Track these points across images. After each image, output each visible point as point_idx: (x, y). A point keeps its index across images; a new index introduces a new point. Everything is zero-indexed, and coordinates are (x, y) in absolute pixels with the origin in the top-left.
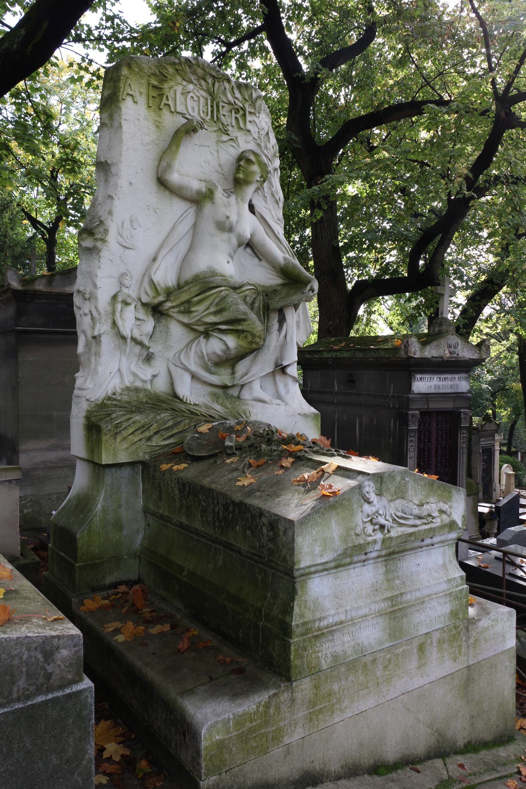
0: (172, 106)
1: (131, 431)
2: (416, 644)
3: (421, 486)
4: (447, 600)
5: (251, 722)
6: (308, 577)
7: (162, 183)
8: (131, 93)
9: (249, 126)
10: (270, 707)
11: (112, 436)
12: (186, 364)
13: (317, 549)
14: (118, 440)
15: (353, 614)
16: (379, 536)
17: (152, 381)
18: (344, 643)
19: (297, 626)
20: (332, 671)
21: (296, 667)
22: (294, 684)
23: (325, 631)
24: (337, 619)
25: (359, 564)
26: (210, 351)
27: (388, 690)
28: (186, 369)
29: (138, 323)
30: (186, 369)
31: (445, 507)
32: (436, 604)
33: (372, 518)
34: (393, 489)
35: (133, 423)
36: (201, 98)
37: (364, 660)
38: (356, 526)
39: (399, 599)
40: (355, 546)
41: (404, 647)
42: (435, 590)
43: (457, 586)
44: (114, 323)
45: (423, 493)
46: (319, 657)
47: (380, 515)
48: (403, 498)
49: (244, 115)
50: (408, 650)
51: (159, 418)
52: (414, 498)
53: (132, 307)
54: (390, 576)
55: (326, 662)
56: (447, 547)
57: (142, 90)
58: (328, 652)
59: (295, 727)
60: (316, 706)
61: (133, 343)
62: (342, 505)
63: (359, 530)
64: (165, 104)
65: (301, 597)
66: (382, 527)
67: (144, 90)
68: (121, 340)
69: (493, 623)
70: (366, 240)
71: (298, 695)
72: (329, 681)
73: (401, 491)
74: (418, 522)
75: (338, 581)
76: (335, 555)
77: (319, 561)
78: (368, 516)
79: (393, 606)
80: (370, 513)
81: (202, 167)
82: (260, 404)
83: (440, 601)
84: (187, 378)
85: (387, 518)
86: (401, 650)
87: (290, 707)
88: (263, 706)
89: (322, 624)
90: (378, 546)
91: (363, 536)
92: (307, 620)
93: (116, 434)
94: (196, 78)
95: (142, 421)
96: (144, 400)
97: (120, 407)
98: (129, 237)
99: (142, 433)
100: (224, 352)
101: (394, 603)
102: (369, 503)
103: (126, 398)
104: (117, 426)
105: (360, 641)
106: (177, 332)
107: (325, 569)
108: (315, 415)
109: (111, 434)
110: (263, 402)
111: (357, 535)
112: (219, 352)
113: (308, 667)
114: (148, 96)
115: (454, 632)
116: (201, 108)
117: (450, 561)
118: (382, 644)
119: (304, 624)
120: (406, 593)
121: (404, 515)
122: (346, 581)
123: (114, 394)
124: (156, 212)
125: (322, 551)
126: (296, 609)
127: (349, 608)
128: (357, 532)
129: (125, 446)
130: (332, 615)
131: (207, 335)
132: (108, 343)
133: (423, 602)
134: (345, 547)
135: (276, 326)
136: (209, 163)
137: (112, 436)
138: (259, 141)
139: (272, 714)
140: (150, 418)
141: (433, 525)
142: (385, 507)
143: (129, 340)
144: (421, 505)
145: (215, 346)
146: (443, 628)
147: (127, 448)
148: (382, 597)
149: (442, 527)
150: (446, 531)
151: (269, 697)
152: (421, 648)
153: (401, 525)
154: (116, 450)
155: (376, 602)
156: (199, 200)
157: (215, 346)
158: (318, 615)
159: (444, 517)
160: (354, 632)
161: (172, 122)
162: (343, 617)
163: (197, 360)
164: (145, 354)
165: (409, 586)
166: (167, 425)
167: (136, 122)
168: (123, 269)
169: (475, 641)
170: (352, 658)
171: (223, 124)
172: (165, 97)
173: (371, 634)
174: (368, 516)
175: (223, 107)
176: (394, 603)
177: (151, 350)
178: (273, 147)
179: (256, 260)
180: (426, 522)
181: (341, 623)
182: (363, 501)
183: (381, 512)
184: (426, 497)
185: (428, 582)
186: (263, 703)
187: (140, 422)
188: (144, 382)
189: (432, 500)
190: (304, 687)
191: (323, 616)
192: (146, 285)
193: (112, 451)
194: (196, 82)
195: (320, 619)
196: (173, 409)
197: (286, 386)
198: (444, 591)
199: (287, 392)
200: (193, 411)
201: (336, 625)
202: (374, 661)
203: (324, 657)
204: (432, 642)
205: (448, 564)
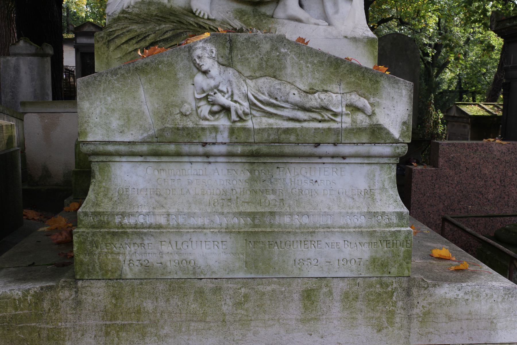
1: (124, 39)
2: (297, 287)
3: (313, 64)
4: (366, 240)
5: (16, 309)
6: (110, 158)
10: (43, 300)
11: (104, 44)
13: (115, 123)
14: (111, 48)
15: (181, 220)
16: (223, 122)
18: (161, 253)
19: (86, 214)
20: (141, 284)
21: (82, 263)
22: (80, 283)
23: (128, 230)
24: (150, 220)
25: (199, 159)
27: (244, 336)
31: (362, 102)
32: (342, 242)
33: (208, 95)
34: (255, 62)
35: (128, 31)
37: (199, 284)
38: (183, 102)
39: (267, 220)
40: (178, 129)
41: (273, 286)
42: (342, 222)
43: (389, 225)
45: (317, 75)
46: (119, 261)
47: (221, 92)
48: (274, 77)
50: (282, 293)
51: (157, 28)
52: (298, 80)
54: (258, 186)
55: (131, 270)
56: (377, 167)
58: (134, 258)
59: (83, 335)
60: (116, 319)
62: (156, 69)
63: (186, 108)
65: (100, 182)
66: (226, 110)
69: (466, 297)
71: (88, 299)
72: (137, 294)
73: (272, 67)
74: (301, 115)
75: (163, 175)
76: (145, 135)
77: (118, 138)
78: (204, 91)
79: (255, 226)
80: (205, 88)
82: (293, 23)
83: (349, 238)
85: (236, 98)
86: (269, 288)
87: (74, 309)
88: (33, 296)
89: (126, 221)
90: (223, 137)
91: (194, 118)
92: (101, 210)
93: (109, 41)
95: (139, 31)
96: (154, 14)
97: (130, 19)
99: (137, 43)
101: (257, 221)
102: (205, 73)
103: (136, 10)
104: (110, 34)
105: (191, 258)
107: (131, 152)
108: (370, 41)
109: (104, 41)
110: (299, 20)
113: (101, 269)
115: (378, 289)
117: (383, 189)
118: (232, 271)
119: (96, 214)
120: (281, 214)
121: (274, 101)
122: (177, 177)
123: (128, 7)
125: (123, 126)
126: (91, 195)
127: (172, 211)
128: (183, 110)
129: (119, 56)
130: (143, 211)
133: (314, 232)
134: (160, 126)
137: (104, 44)
139: (47, 310)
140: (148, 28)
141: (334, 125)
142: (230, 81)
144: (312, 91)
146: (354, 278)
147: (121, 58)
148: (236, 210)
149: (356, 130)
150: (364, 139)
151: (42, 288)
152: (309, 296)
153: (270, 115)
154: (109, 58)
155: (223, 214)
158: (120, 209)
159: (360, 117)
160: (179, 243)
162: (162, 221)
165: (290, 206)
166: (166, 36)
169: (427, 314)
170: (176, 277)
173: (211, 254)
176: (257, 221)
180: (320, 118)
181: (160, 227)
182: (195, 70)
183: (223, 88)
184: (323, 81)
185: (329, 208)
186: (32, 292)
187: (136, 31)
189: (335, 87)
190: (96, 292)
191: (128, 211)
193: (105, 60)
196: (180, 22)
198: (360, 227)
199: (337, 12)
200: (202, 24)
201: (149, 227)
202: (217, 290)
203: (127, 262)
204: (331, 293)
205: (377, 192)
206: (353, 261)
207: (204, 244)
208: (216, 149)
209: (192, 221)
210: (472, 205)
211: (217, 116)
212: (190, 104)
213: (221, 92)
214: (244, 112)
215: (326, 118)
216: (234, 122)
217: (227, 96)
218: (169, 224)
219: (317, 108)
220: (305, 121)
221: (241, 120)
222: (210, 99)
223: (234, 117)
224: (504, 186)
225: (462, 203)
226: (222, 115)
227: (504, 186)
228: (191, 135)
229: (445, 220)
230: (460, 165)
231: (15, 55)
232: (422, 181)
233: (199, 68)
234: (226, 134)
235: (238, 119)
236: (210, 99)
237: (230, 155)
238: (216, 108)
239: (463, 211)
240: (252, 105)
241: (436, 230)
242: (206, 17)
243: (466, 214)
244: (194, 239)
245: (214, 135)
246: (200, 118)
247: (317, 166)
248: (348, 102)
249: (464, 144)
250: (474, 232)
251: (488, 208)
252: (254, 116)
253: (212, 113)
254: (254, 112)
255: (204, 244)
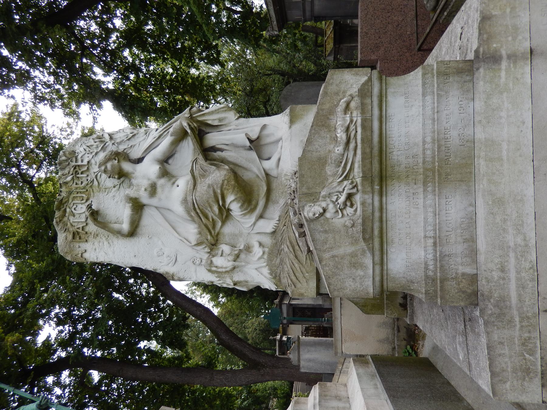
0: (82, 225)
7: (132, 233)
8: (80, 255)
9: (85, 162)
12: (251, 224)
16: (358, 198)
17: (263, 247)
26: (240, 210)
28: (254, 224)
29: (224, 254)
30: (254, 224)
32: (445, 112)
33: (339, 208)
36: (74, 202)
44: (226, 272)
47: (337, 200)
49: (79, 166)
53: (214, 259)
57: (77, 246)
61: (238, 260)
63: (348, 223)
64: (83, 230)
66: (350, 197)
67: (77, 245)
68: (236, 269)
70: (74, 308)
74: (352, 146)
75: (396, 240)
77: (371, 271)
78: (337, 211)
80: (334, 210)
81: (117, 202)
84: (261, 222)
85: (341, 190)
94: (62, 206)
98: (169, 258)
100: (238, 202)
102: (325, 210)
106: (228, 229)
110: (279, 160)
111: (353, 225)
112: (240, 205)
114: (80, 242)
116: (80, 202)
124: (151, 238)
128: (350, 225)
131: (229, 210)
132: (238, 277)
135: (219, 153)
136: (114, 196)
138: (94, 154)
143: (236, 264)
144: (335, 139)
145: (235, 208)
149: (363, 108)
153: (353, 163)
156: (138, 207)
157: (235, 208)
159: (353, 105)
160: (448, 229)
161: (92, 227)
163: (247, 217)
164: (245, 252)
166: (292, 250)
167: (97, 250)
168: (190, 263)
171: (87, 184)
172: (78, 230)
174: (337, 211)
175: (76, 184)
177: (242, 247)
178: (95, 142)
179: (176, 155)
181: (435, 244)
183: (334, 198)
188: (264, 253)
192: (199, 248)
194: (65, 205)
195: (426, 264)
197: (268, 136)
206: (461, 103)
207: (448, 212)
208: (377, 204)
209: (430, 219)
210: (407, 31)
211: (354, 202)
212: (346, 222)
213: (337, 200)
214: (350, 184)
215: (354, 127)
216: (358, 190)
217: (340, 196)
218: (433, 237)
219: (347, 135)
220: (356, 142)
221: (356, 186)
222: (342, 207)
223: (354, 190)
224: (392, 9)
225: (405, 39)
226: (353, 199)
227: (392, 9)
228: (366, 222)
229: (419, 50)
230: (376, 43)
231: (299, 360)
232: (388, 69)
233: (322, 215)
234: (366, 196)
235: (356, 188)
236: (342, 207)
237: (381, 195)
238: (348, 204)
239: (411, 38)
240: (346, 178)
241: (429, 54)
242: (278, 222)
243: (415, 35)
244: (445, 219)
245: (367, 205)
246: (355, 214)
247: (388, 133)
248: (343, 113)
249: (361, 42)
250: (430, 26)
251: (409, 19)
252: (353, 177)
253: (352, 206)
254: (351, 177)
255: (448, 212)
